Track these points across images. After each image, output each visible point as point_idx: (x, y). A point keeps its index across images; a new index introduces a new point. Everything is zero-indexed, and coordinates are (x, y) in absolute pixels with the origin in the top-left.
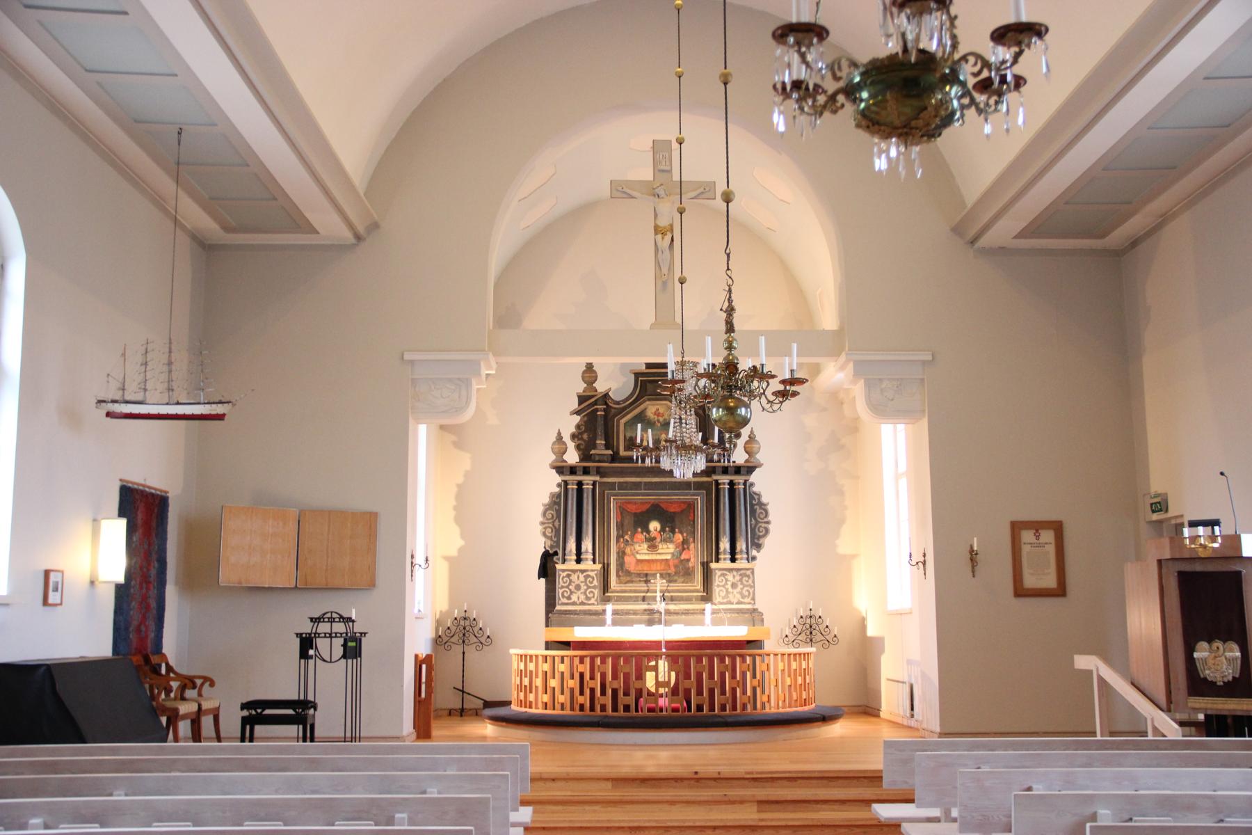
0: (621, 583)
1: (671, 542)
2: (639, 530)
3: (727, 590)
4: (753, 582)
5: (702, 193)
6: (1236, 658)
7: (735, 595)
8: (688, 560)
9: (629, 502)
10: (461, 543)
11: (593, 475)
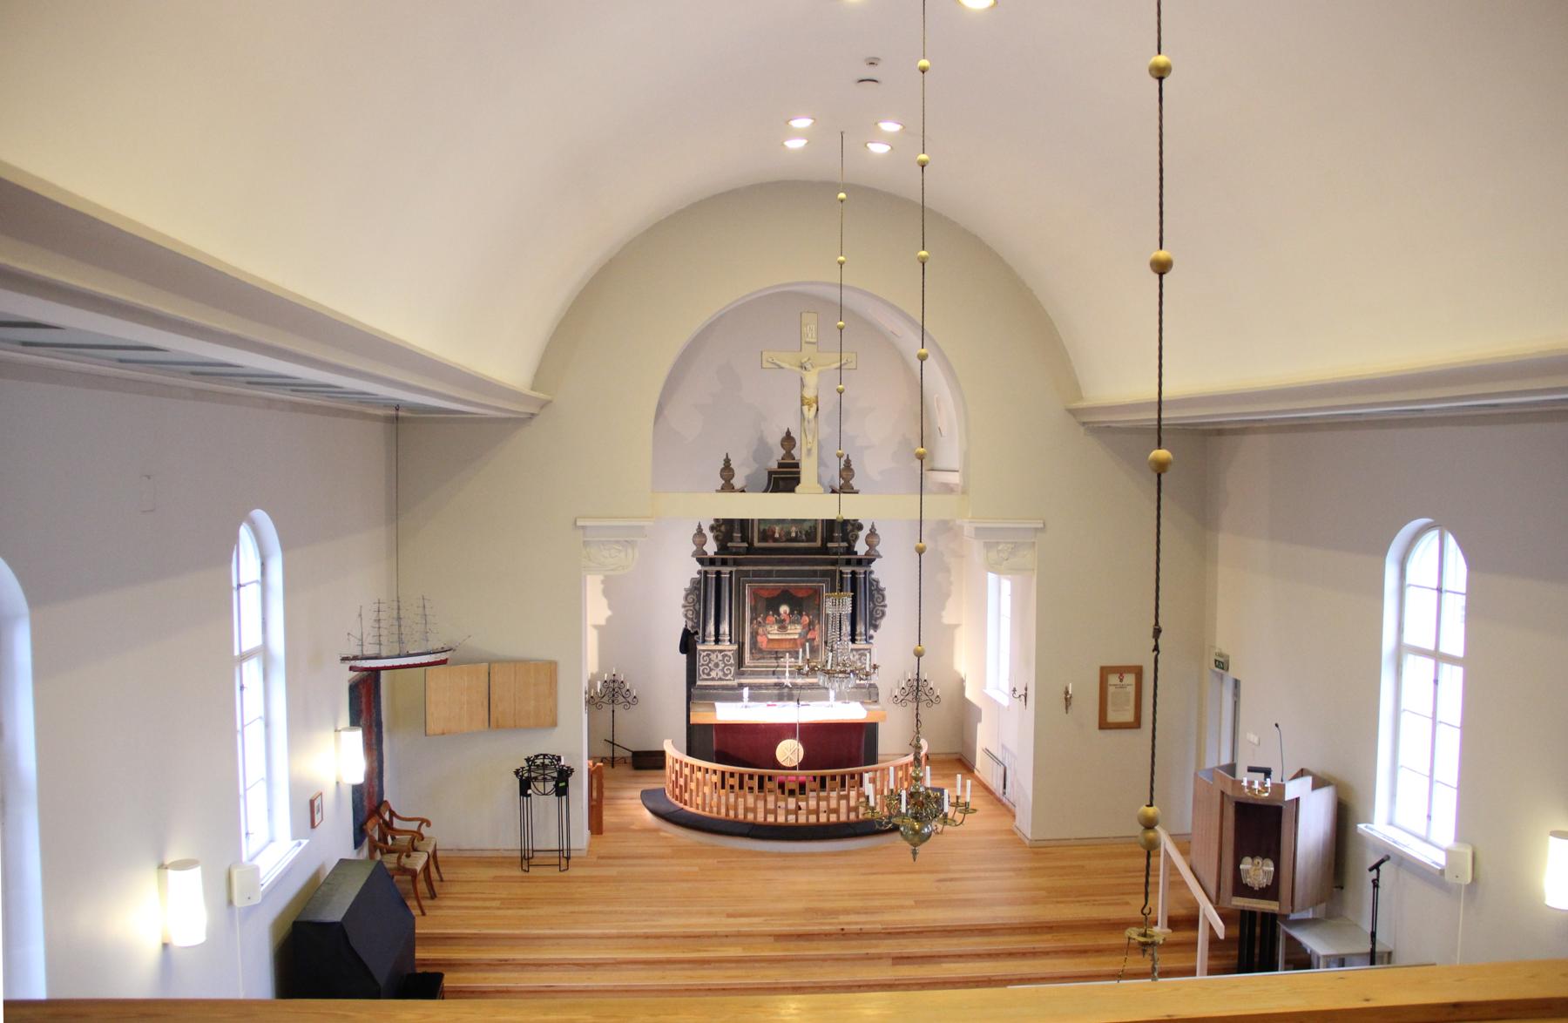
0: (754, 659)
1: (799, 623)
2: (771, 613)
8: (814, 639)
9: (762, 588)
10: (609, 613)
11: (730, 566)
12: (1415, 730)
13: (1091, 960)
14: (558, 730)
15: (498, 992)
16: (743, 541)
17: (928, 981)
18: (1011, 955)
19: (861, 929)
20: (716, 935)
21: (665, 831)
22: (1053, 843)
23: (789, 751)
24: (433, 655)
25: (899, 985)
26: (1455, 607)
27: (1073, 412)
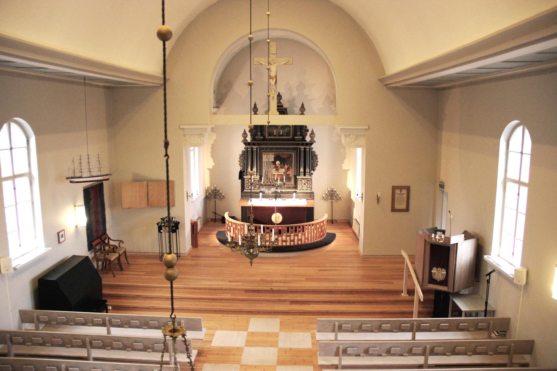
1: (284, 168)
3: (302, 185)
4: (311, 183)
5: (287, 62)
6: (444, 274)
7: (305, 187)
8: (289, 174)
10: (213, 164)
11: (256, 146)
12: (510, 215)
13: (373, 306)
14: (175, 207)
15: (134, 308)
16: (261, 136)
17: (302, 312)
18: (339, 302)
19: (279, 289)
20: (221, 289)
21: (222, 247)
22: (371, 257)
23: (277, 218)
24: (103, 177)
25: (290, 313)
26: (527, 159)
27: (381, 80)
